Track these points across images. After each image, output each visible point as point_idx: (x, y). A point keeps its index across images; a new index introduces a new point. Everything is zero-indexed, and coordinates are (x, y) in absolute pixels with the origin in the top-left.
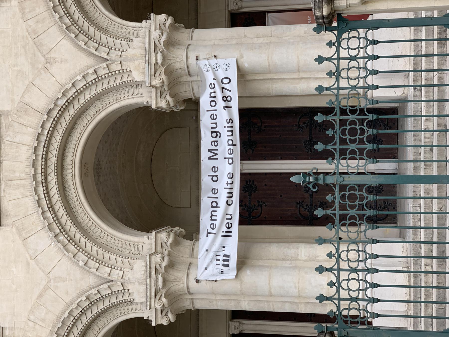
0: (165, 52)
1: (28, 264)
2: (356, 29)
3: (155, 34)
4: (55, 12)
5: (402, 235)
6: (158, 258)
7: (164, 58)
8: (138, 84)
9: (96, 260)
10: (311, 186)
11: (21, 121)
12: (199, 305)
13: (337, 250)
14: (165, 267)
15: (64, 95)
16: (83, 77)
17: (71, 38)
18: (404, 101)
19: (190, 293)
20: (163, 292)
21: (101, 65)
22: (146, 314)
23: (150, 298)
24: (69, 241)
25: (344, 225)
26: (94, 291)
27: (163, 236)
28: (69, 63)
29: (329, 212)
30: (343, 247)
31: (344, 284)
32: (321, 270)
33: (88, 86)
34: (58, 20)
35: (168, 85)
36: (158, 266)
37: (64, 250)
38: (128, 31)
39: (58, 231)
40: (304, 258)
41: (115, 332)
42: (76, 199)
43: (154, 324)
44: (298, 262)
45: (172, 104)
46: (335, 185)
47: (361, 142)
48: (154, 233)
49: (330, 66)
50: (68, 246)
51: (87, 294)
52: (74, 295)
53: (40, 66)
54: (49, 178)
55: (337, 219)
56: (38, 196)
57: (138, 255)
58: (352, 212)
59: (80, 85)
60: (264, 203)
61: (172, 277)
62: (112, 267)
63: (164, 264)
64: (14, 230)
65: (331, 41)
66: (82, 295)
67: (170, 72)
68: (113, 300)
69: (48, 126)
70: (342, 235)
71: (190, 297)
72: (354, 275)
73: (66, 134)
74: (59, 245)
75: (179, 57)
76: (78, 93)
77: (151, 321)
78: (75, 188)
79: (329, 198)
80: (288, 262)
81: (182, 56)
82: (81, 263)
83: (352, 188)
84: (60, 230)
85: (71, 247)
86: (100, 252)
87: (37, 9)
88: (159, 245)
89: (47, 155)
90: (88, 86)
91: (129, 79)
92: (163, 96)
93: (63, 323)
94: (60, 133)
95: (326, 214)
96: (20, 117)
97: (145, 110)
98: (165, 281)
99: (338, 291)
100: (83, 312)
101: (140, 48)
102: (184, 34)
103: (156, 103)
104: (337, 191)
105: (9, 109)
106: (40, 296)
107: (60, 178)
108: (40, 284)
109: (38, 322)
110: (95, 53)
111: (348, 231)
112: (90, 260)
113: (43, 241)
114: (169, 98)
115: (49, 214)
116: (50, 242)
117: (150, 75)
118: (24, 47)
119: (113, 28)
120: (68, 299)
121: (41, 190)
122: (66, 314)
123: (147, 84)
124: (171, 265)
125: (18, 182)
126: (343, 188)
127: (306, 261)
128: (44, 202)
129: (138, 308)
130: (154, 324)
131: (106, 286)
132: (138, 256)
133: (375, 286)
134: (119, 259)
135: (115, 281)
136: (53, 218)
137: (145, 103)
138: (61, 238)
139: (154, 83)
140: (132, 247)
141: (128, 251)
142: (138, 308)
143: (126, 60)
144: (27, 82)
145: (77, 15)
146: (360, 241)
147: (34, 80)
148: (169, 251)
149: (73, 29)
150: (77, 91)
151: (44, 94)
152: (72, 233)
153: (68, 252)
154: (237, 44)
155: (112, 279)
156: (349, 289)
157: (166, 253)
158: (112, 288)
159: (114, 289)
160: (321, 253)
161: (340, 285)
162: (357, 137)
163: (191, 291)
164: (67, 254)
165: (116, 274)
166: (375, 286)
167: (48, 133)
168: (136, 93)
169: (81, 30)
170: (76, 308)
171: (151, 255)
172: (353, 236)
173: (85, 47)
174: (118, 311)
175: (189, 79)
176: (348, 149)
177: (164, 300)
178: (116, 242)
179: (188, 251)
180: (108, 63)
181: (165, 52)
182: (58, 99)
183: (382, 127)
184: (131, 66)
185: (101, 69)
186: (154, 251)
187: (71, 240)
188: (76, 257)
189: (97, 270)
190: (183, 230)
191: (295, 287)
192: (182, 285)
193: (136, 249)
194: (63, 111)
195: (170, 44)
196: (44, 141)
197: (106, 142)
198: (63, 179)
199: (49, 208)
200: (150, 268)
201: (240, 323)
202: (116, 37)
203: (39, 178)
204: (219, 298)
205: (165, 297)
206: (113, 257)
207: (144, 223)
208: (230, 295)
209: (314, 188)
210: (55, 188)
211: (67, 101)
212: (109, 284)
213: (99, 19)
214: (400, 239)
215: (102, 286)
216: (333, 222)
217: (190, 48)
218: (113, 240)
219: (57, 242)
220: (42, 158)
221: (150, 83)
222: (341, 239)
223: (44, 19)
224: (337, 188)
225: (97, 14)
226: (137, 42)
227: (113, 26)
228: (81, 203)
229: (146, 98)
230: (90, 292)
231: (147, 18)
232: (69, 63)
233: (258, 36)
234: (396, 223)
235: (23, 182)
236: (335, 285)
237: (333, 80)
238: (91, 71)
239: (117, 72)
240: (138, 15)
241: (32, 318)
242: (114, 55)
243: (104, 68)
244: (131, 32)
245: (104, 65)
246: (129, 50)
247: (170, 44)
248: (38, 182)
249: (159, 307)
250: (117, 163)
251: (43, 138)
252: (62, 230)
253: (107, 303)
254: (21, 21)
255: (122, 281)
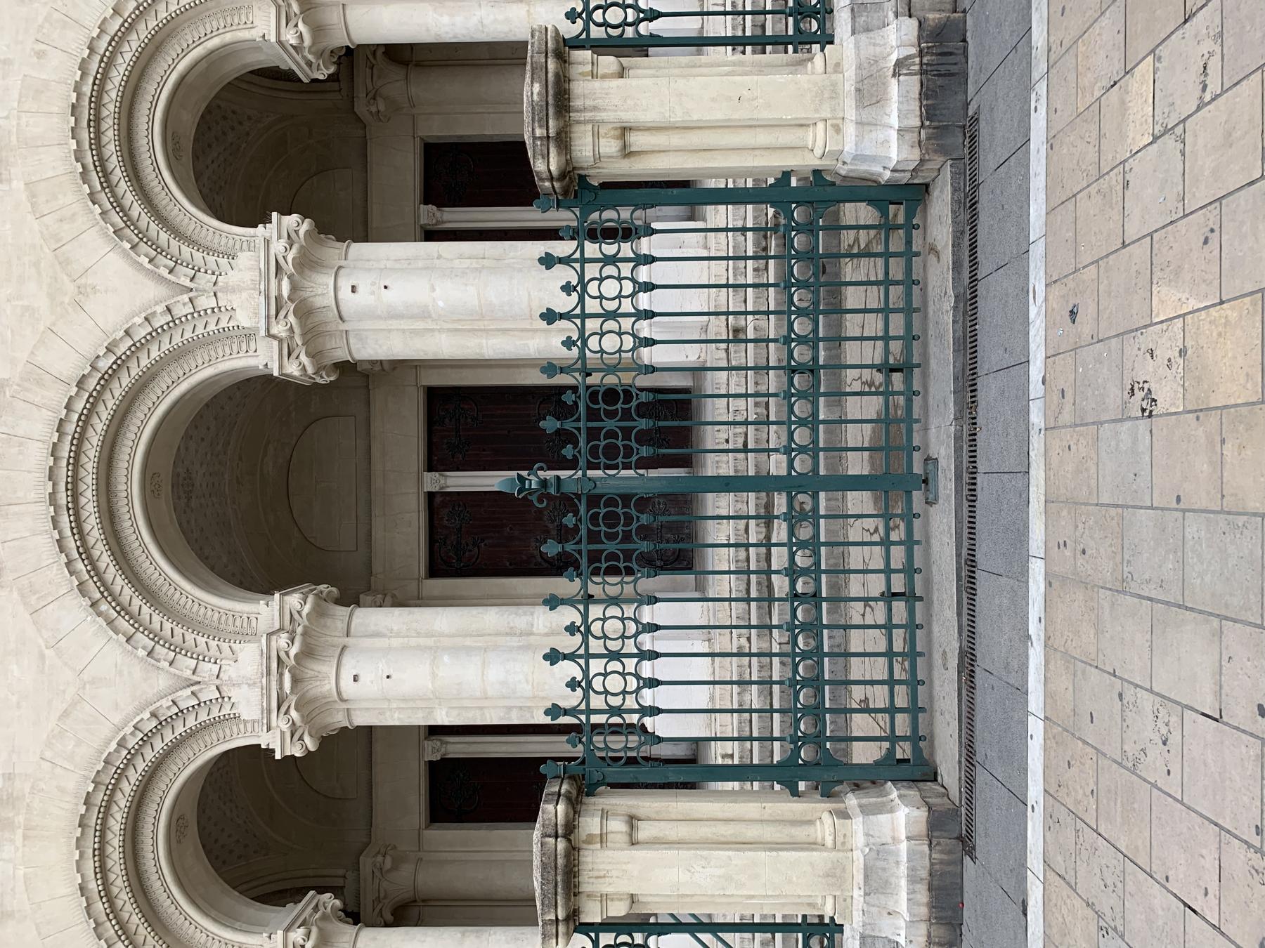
0: (297, 277)
1: (42, 657)
2: (614, 207)
3: (278, 247)
4: (94, 203)
5: (700, 587)
6: (282, 640)
7: (294, 288)
8: (250, 335)
9: (171, 647)
10: (534, 498)
11: (30, 397)
12: (361, 720)
13: (585, 616)
14: (296, 656)
15: (109, 350)
16: (146, 319)
17: (124, 250)
18: (698, 371)
19: (342, 700)
20: (293, 700)
21: (179, 298)
22: (264, 740)
23: (269, 712)
24: (119, 613)
25: (596, 572)
26: (166, 702)
27: (294, 600)
28: (114, 291)
29: (570, 547)
30: (595, 611)
31: (597, 684)
32: (554, 657)
33: (154, 335)
34: (98, 217)
35: (303, 335)
36: (283, 655)
37: (108, 629)
38: (231, 242)
39: (98, 596)
40: (543, 630)
41: (210, 774)
42: (134, 537)
43: (278, 756)
44: (532, 638)
45: (310, 370)
46: (579, 496)
47: (626, 415)
48: (277, 596)
49: (570, 670)
50: (116, 623)
51: (152, 708)
52: (131, 708)
53: (67, 300)
54: (83, 501)
55: (584, 562)
56: (60, 533)
57: (248, 635)
58: (611, 547)
59: (140, 333)
60: (483, 540)
61: (311, 673)
62: (200, 658)
63: (294, 651)
64: (15, 595)
65: (569, 283)
66: (142, 710)
67: (305, 312)
68: (203, 717)
69: (79, 405)
70: (594, 589)
71: (345, 706)
72: (615, 665)
73: (116, 421)
74: (100, 620)
75: (321, 288)
76: (137, 348)
77: (273, 751)
78: (133, 518)
79: (569, 520)
80: (515, 639)
81: (327, 285)
82: (142, 653)
83: (611, 502)
84: (102, 593)
85: (123, 624)
86: (178, 631)
87: (60, 196)
88: (287, 617)
89: (77, 459)
90: (154, 335)
91: (230, 325)
92: (294, 355)
93: (107, 762)
94: (104, 419)
95: (565, 552)
96: (27, 390)
97: (266, 380)
98: (295, 681)
99: (586, 697)
100: (146, 740)
101: (250, 269)
102: (333, 251)
103: (281, 367)
104: (582, 509)
105: (7, 377)
106: (65, 714)
107: (103, 499)
108: (64, 692)
109: (59, 761)
110: (169, 277)
111: (605, 582)
112: (158, 646)
113: (73, 615)
114: (304, 359)
115: (80, 566)
116: (83, 615)
117: (268, 317)
118: (36, 265)
119: (205, 237)
120: (117, 719)
121: (65, 520)
122: (113, 746)
123: (262, 333)
124: (308, 652)
125: (22, 508)
126: (594, 500)
127: (547, 635)
128: (71, 544)
129: (249, 729)
130: (278, 756)
131: (188, 692)
132: (248, 638)
133: (653, 683)
134: (213, 644)
135: (205, 683)
136: (88, 572)
137: (261, 367)
138: (104, 607)
139: (274, 331)
140: (238, 622)
141: (231, 628)
142: (249, 729)
143: (226, 289)
144: (42, 328)
145: (136, 210)
146: (629, 601)
147: (54, 324)
148: (305, 627)
149: (128, 232)
150: (134, 345)
151: (72, 351)
152: (125, 599)
153: (116, 632)
154: (427, 268)
155: (199, 679)
156: (606, 692)
157: (299, 630)
158: (199, 695)
159: (204, 697)
160: (549, 624)
161: (589, 684)
162: (619, 406)
163: (345, 696)
164: (115, 636)
165: (208, 669)
166: (653, 683)
167: (79, 420)
168: (244, 348)
169: (143, 236)
170: (132, 734)
171: (270, 635)
172: (613, 591)
173: (150, 266)
174: (214, 736)
175: (343, 327)
176: (601, 429)
177: (294, 714)
178: (210, 612)
179: (341, 625)
180: (191, 294)
181: (297, 277)
182: (98, 357)
183: (665, 418)
184: (235, 300)
185: (180, 306)
186: (277, 626)
187: (123, 610)
188: (132, 642)
189: (171, 664)
190: (334, 589)
191: (527, 681)
192: (330, 686)
193: (245, 625)
194: (108, 379)
195: (307, 263)
196: (71, 432)
197: (203, 439)
198: (109, 501)
199: (80, 554)
200: (269, 658)
201: (442, 743)
202: (208, 250)
203: (63, 498)
204: (395, 705)
205: (297, 709)
206: (202, 640)
207: (260, 578)
208: (413, 700)
209: (540, 501)
210: (93, 517)
211: (115, 362)
212: (193, 688)
213: (178, 219)
214: (697, 595)
215: (180, 693)
216: (577, 567)
217: (342, 272)
218: (203, 609)
219: (95, 615)
220: (68, 464)
221: (268, 330)
222: (591, 596)
223: (74, 215)
224: (584, 500)
225: (176, 211)
226: (244, 259)
227: (204, 231)
228: (143, 544)
229: (263, 358)
230: (158, 704)
231: (266, 220)
232: (114, 291)
233: (461, 257)
234: (691, 569)
235: (32, 508)
236: (580, 686)
237: (578, 638)
238: (160, 308)
239: (209, 311)
240: (248, 213)
241: (48, 755)
242: (204, 280)
243: (184, 304)
244: (238, 243)
245: (185, 298)
246: (230, 273)
247: (307, 263)
248: (60, 507)
249: (285, 727)
250: (226, 476)
251: (70, 428)
252: (106, 594)
253: (191, 722)
254: (30, 217)
255: (218, 682)
